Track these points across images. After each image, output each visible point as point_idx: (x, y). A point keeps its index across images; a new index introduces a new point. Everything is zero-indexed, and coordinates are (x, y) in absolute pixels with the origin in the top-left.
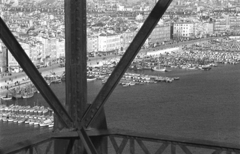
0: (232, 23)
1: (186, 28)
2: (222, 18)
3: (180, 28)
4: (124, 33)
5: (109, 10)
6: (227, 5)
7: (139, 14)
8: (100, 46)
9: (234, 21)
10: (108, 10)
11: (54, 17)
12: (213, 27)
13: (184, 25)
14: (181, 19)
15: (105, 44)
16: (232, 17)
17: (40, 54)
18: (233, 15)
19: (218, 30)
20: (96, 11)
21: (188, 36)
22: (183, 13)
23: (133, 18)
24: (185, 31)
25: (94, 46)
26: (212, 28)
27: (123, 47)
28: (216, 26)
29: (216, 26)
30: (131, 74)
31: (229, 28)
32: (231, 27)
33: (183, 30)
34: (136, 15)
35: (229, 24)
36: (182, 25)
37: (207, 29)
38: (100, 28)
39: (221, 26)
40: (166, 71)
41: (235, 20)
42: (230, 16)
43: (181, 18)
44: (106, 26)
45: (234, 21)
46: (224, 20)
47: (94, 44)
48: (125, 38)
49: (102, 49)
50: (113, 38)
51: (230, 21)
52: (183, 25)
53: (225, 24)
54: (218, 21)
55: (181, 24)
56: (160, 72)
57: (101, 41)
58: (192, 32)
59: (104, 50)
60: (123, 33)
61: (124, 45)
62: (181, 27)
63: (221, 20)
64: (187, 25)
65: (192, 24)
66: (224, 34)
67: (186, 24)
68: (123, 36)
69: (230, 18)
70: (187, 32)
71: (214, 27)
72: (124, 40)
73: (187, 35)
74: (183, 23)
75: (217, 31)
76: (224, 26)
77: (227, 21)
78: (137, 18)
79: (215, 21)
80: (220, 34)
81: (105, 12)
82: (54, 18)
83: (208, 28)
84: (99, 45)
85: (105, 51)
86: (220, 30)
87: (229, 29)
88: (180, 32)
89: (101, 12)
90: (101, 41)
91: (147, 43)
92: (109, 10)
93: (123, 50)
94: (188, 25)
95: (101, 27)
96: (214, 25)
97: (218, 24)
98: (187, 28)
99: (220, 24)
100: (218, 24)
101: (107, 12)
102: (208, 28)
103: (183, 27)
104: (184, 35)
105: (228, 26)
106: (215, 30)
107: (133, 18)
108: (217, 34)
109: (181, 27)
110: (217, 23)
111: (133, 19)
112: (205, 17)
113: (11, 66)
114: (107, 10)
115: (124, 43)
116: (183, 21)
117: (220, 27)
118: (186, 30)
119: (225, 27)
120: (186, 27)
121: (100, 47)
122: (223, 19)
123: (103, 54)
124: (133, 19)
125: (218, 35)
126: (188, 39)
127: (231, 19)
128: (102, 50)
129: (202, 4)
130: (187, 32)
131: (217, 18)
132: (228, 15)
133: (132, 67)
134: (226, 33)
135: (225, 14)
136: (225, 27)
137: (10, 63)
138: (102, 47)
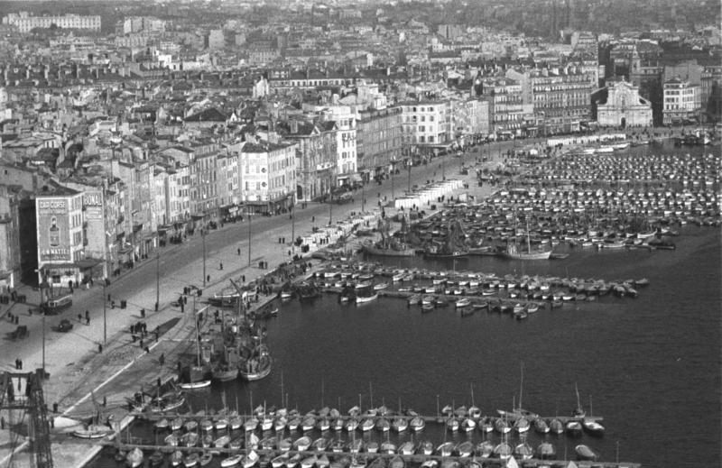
0: (540, 97)
1: (427, 118)
2: (511, 82)
3: (408, 119)
4: (304, 138)
5: (151, 69)
6: (429, 45)
7: (260, 78)
8: (247, 183)
9: (543, 92)
10: (149, 68)
11: (9, 97)
12: (490, 111)
13: (423, 110)
14: (408, 90)
15: (264, 178)
16: (537, 80)
17: (121, 220)
18: (541, 75)
19: (502, 121)
20: (113, 71)
21: (437, 141)
22: (384, 72)
23: (245, 90)
24: (427, 129)
25: (231, 186)
26: (486, 116)
27: (303, 186)
28: (497, 107)
29: (497, 107)
30: (473, 276)
31: (531, 115)
32: (536, 111)
33: (420, 123)
34: (253, 83)
35: (530, 103)
36: (415, 110)
37: (474, 122)
38: (215, 126)
39: (509, 108)
40: (551, 258)
41: (548, 89)
42: (532, 76)
43: (407, 86)
44: (231, 120)
45: (543, 92)
46: (519, 88)
47: (230, 180)
48: (308, 156)
49: (253, 194)
50: (281, 156)
51: (535, 91)
52: (419, 107)
53: (521, 102)
54: (500, 94)
55: (411, 107)
56: (537, 261)
57: (247, 167)
58: (444, 131)
59: (259, 197)
60: (302, 142)
61: (306, 179)
62: (412, 114)
63: (509, 89)
64: (432, 109)
65: (444, 105)
66: (519, 132)
67: (430, 106)
68: (302, 151)
69: (533, 84)
70: (431, 129)
71: (491, 113)
72: (306, 163)
73: (431, 139)
74: (418, 103)
75: (501, 122)
76: (518, 107)
77: (525, 93)
78: (256, 91)
79: (493, 94)
80: (510, 132)
81: (141, 74)
82: (6, 99)
83: (476, 114)
84: (244, 181)
85: (264, 199)
86: (507, 120)
87: (533, 118)
88: (408, 129)
89: (129, 75)
90: (247, 167)
91: (356, 171)
92: (151, 69)
93: (304, 195)
94: (436, 107)
95: (219, 124)
96: (492, 104)
97: (501, 103)
98: (432, 119)
99: (508, 103)
100: (501, 103)
101: (147, 74)
102: (476, 114)
103: (419, 114)
104: (423, 138)
105: (529, 109)
106: (493, 123)
107: (245, 90)
108: (499, 134)
109: (412, 114)
110: (498, 99)
111: (242, 94)
112: (460, 82)
113: (46, 266)
114: (147, 70)
115: (306, 173)
116: (413, 95)
117: (507, 112)
118: (427, 124)
119: (522, 110)
120: (427, 114)
121: (247, 189)
122: (516, 87)
123: (257, 212)
124: (242, 94)
125: (503, 137)
126: (436, 152)
127: (535, 84)
128: (253, 199)
129: (352, 43)
130: (431, 129)
131: (498, 84)
132: (526, 76)
133: (432, 251)
134: (524, 129)
135: (517, 71)
136: (522, 110)
137: (43, 257)
138: (252, 188)
